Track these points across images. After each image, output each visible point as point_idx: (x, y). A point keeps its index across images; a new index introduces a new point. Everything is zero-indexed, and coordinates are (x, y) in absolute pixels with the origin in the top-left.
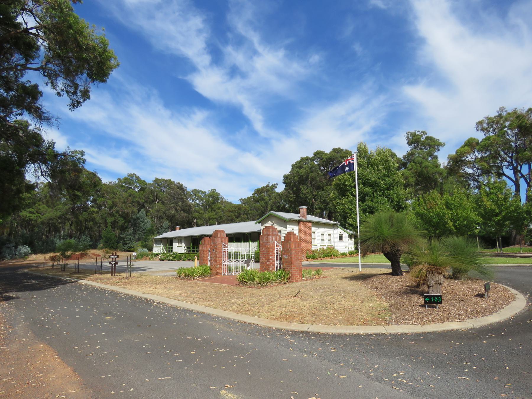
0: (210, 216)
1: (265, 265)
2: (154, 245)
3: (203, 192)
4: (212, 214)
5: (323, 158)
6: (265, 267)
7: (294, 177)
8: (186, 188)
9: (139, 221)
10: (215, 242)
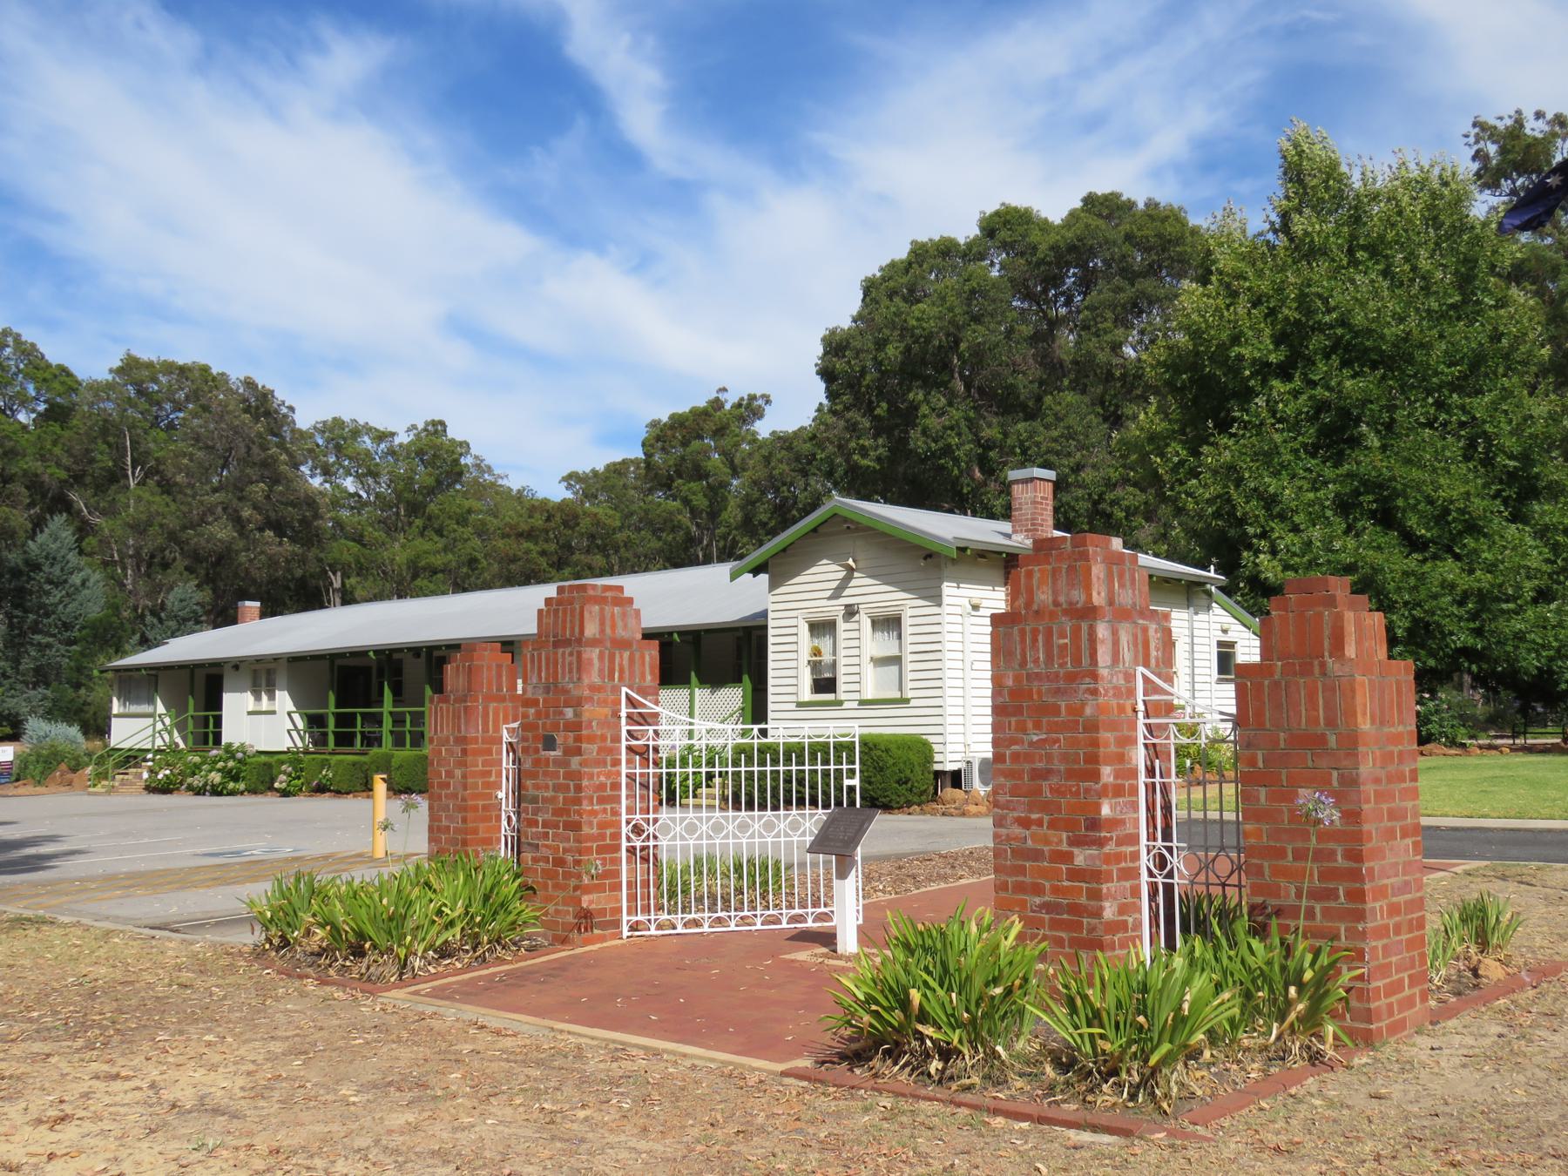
0: (418, 556)
1: (1056, 874)
2: (116, 707)
3: (381, 436)
4: (428, 548)
5: (1035, 248)
6: (1056, 890)
7: (881, 344)
8: (292, 409)
9: (40, 577)
10: (565, 681)
